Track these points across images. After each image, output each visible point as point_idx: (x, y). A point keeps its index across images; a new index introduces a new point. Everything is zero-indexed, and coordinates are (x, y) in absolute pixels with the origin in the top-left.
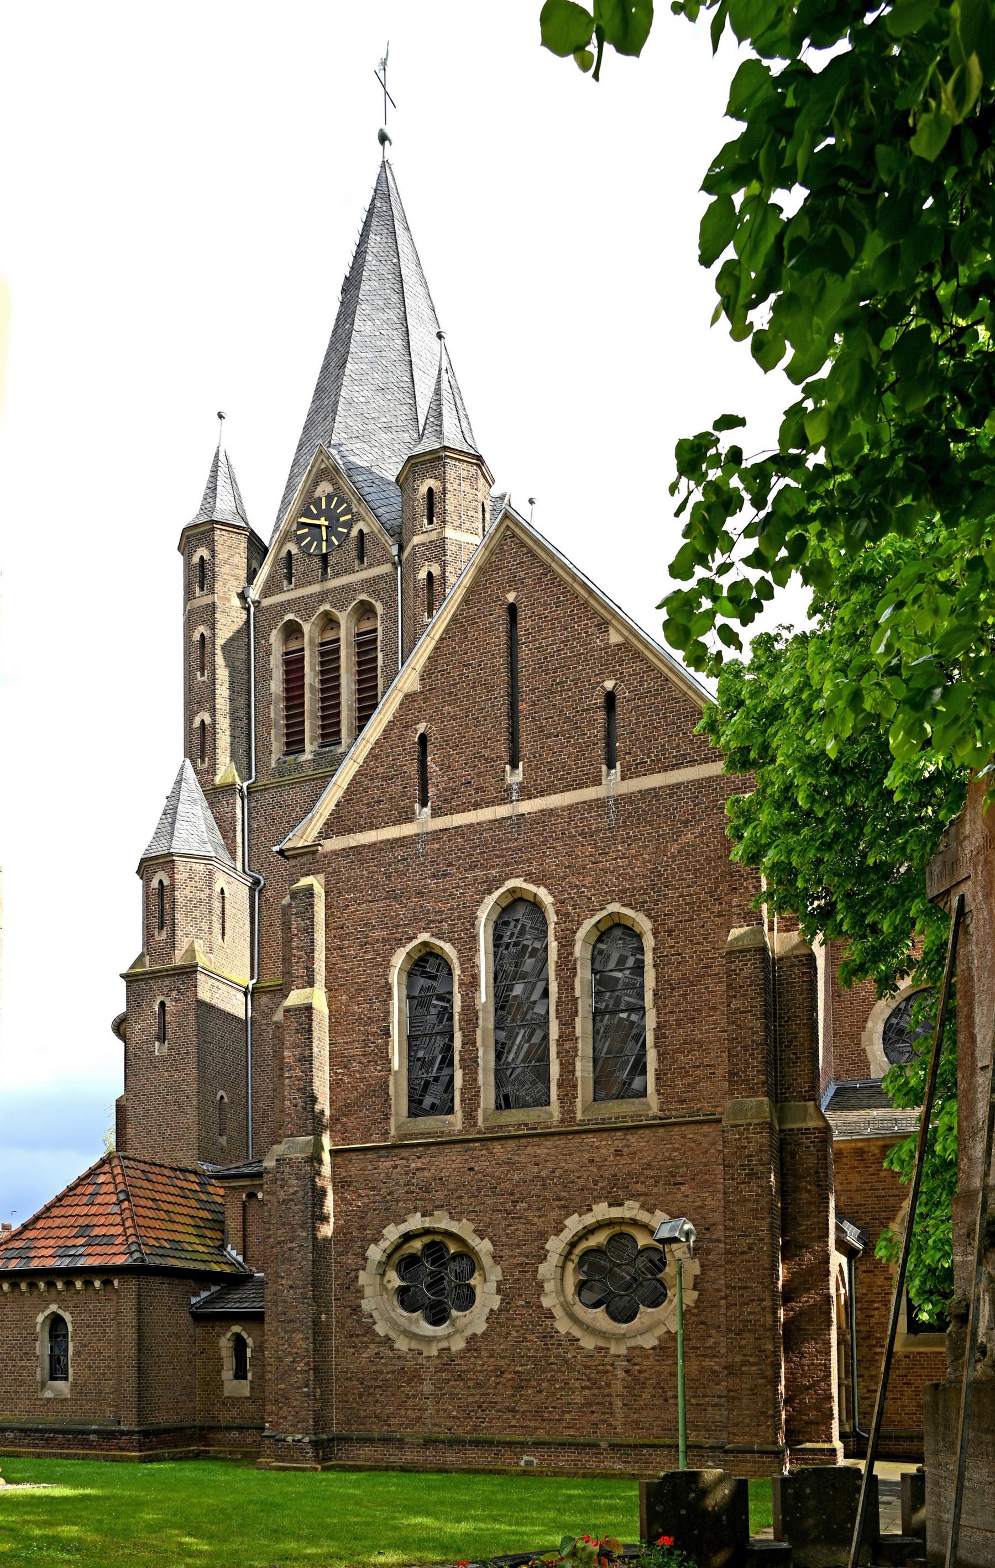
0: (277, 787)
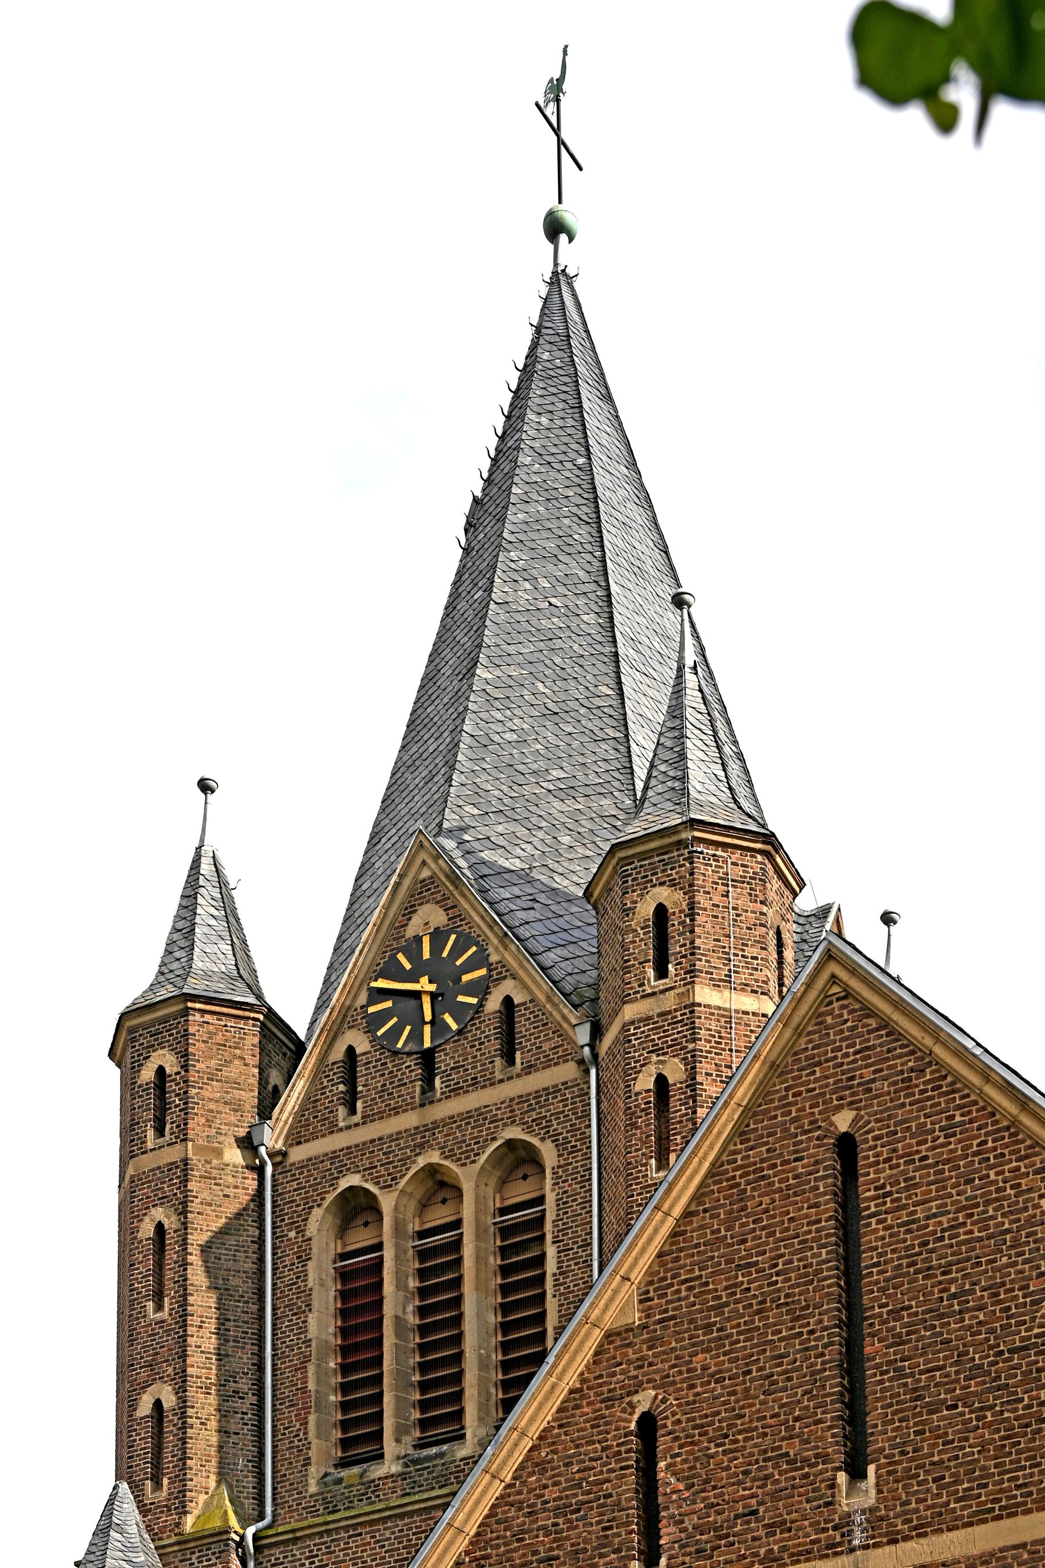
0: (321, 1534)
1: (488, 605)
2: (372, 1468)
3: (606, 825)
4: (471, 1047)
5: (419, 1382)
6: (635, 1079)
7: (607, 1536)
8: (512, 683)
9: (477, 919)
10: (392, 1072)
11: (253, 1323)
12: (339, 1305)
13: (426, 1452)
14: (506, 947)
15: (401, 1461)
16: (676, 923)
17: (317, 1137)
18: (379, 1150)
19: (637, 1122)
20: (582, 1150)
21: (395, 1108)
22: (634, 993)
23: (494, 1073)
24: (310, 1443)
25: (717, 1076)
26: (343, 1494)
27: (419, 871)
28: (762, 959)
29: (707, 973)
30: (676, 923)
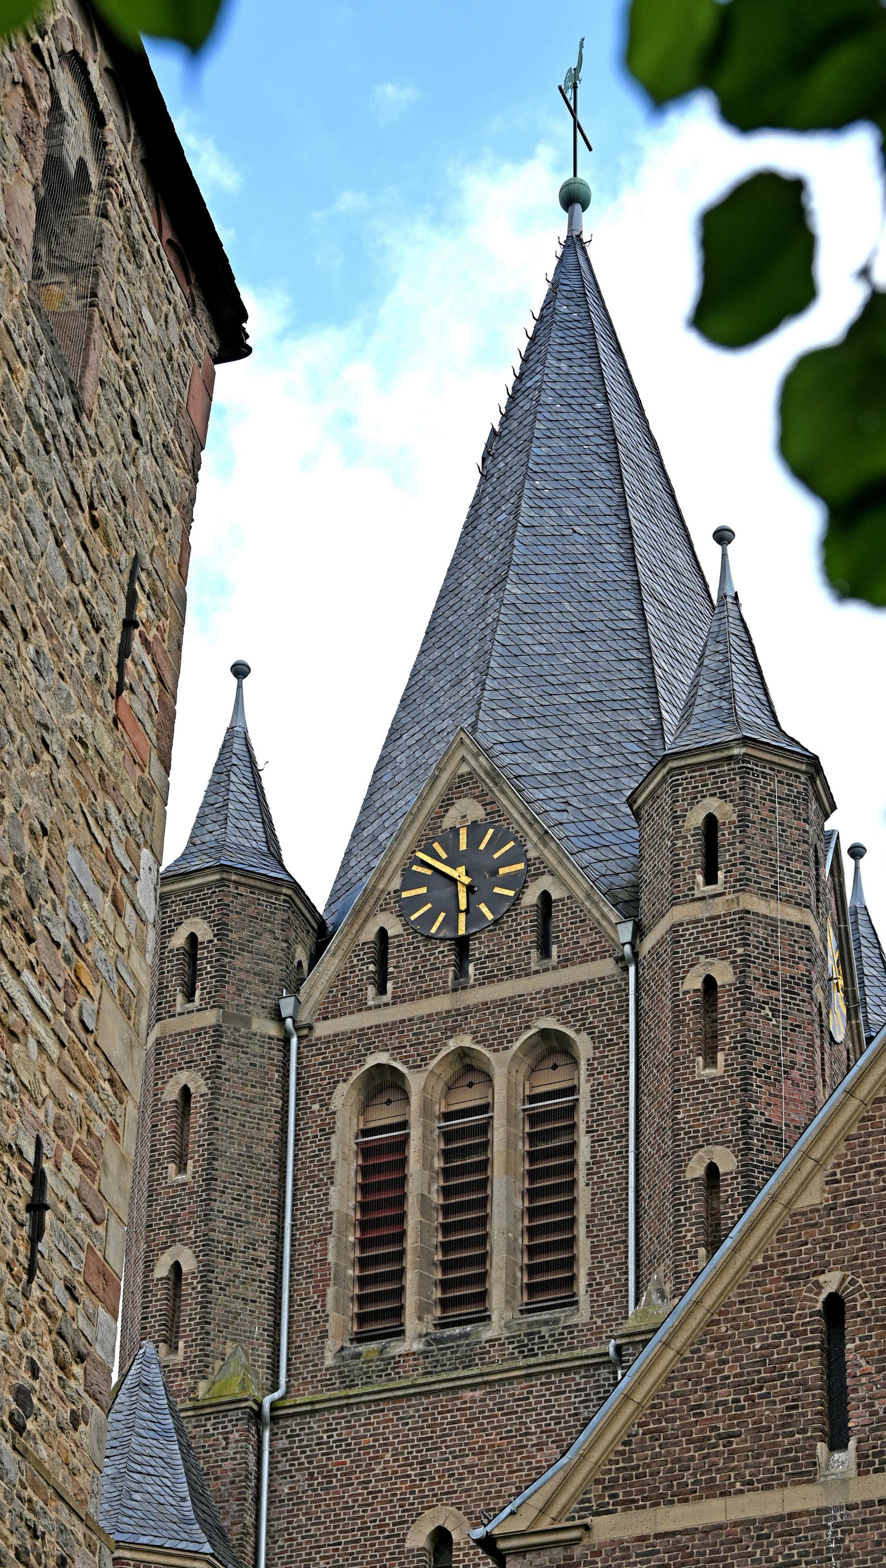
0: (340, 1408)
1: (515, 527)
2: (392, 1344)
3: (632, 739)
4: (507, 937)
5: (442, 1262)
6: (683, 978)
7: (791, 1416)
8: (540, 600)
9: (517, 816)
10: (425, 956)
11: (273, 1192)
12: (360, 1180)
13: (448, 1332)
14: (545, 845)
15: (423, 1339)
16: (726, 832)
17: (345, 1014)
18: (408, 1031)
19: (684, 1020)
20: (618, 1044)
21: (426, 991)
22: (684, 896)
23: (529, 963)
24: (327, 1316)
25: (764, 981)
26: (361, 1368)
27: (458, 766)
28: (805, 874)
29: (755, 882)
30: (726, 832)
